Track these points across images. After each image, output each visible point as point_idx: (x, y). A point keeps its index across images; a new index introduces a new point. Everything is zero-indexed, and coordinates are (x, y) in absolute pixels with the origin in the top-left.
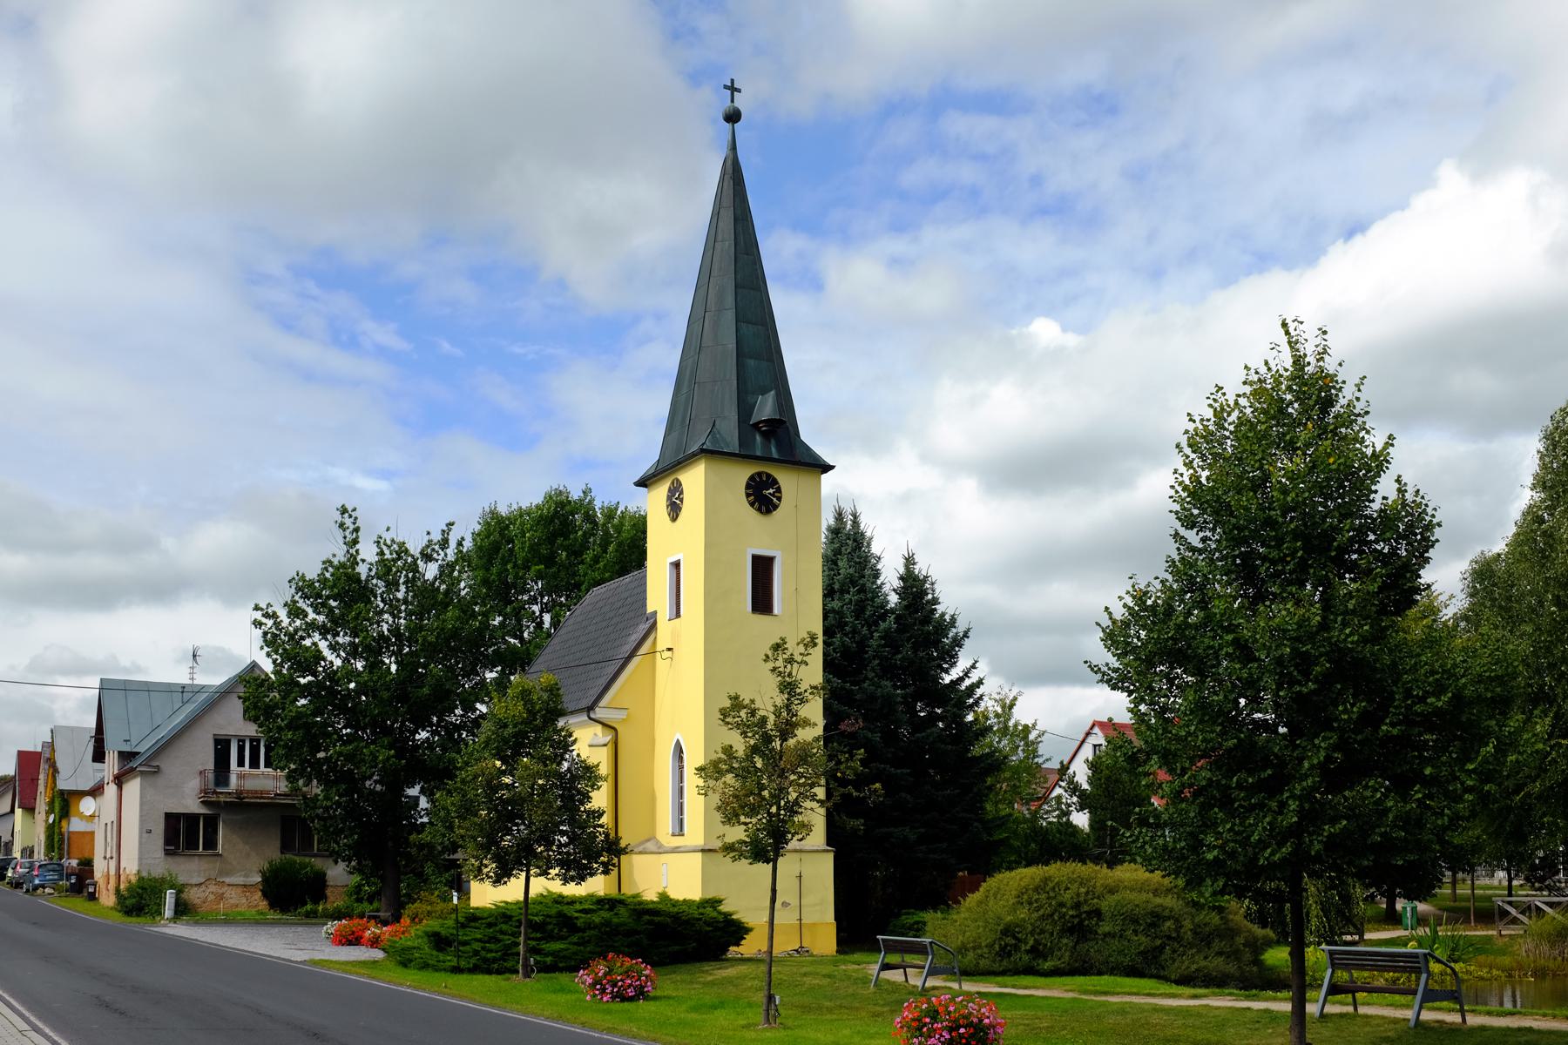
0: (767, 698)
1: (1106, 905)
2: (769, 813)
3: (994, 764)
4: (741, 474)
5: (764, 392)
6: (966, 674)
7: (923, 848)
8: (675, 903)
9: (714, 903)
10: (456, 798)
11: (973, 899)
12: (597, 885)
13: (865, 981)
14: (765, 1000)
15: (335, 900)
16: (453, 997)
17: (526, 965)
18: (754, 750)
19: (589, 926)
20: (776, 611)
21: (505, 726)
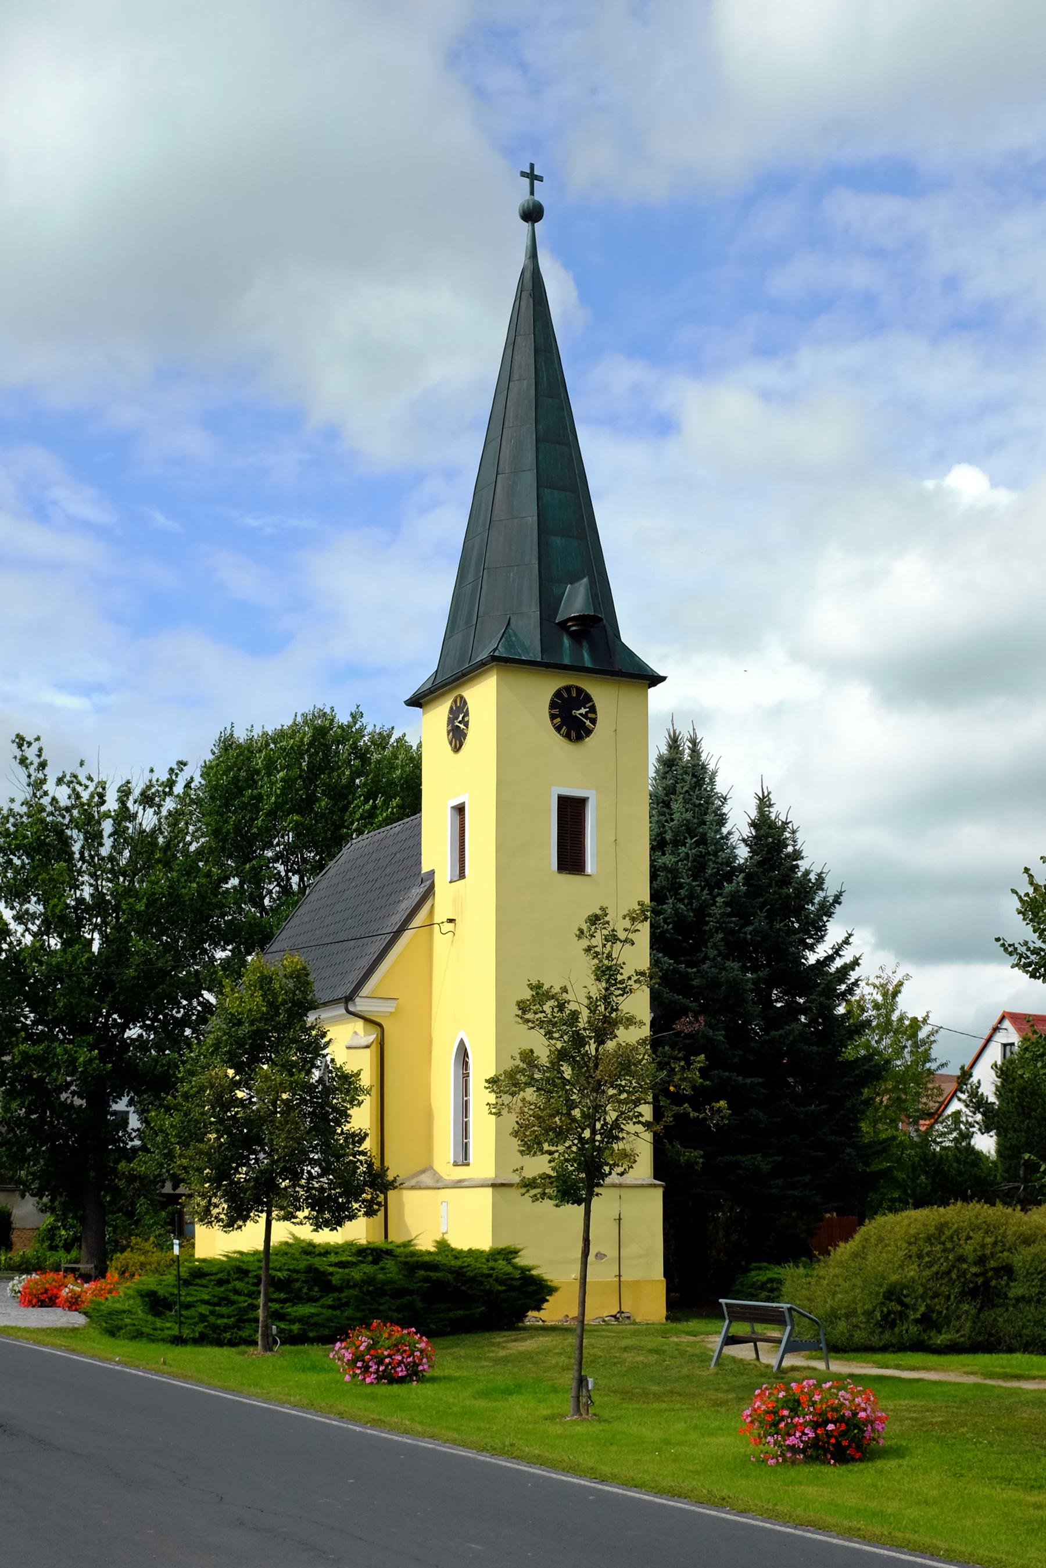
0: (581, 988)
1: (1020, 1259)
2: (581, 1139)
3: (873, 1070)
4: (543, 689)
5: (574, 579)
6: (837, 952)
7: (780, 1182)
8: (458, 1254)
9: (508, 1254)
10: (176, 1118)
11: (844, 1250)
12: (357, 1231)
13: (704, 1358)
14: (574, 1384)
15: (24, 1248)
16: (175, 1377)
17: (266, 1335)
18: (562, 1055)
19: (347, 1284)
20: (589, 869)
21: (240, 1023)
